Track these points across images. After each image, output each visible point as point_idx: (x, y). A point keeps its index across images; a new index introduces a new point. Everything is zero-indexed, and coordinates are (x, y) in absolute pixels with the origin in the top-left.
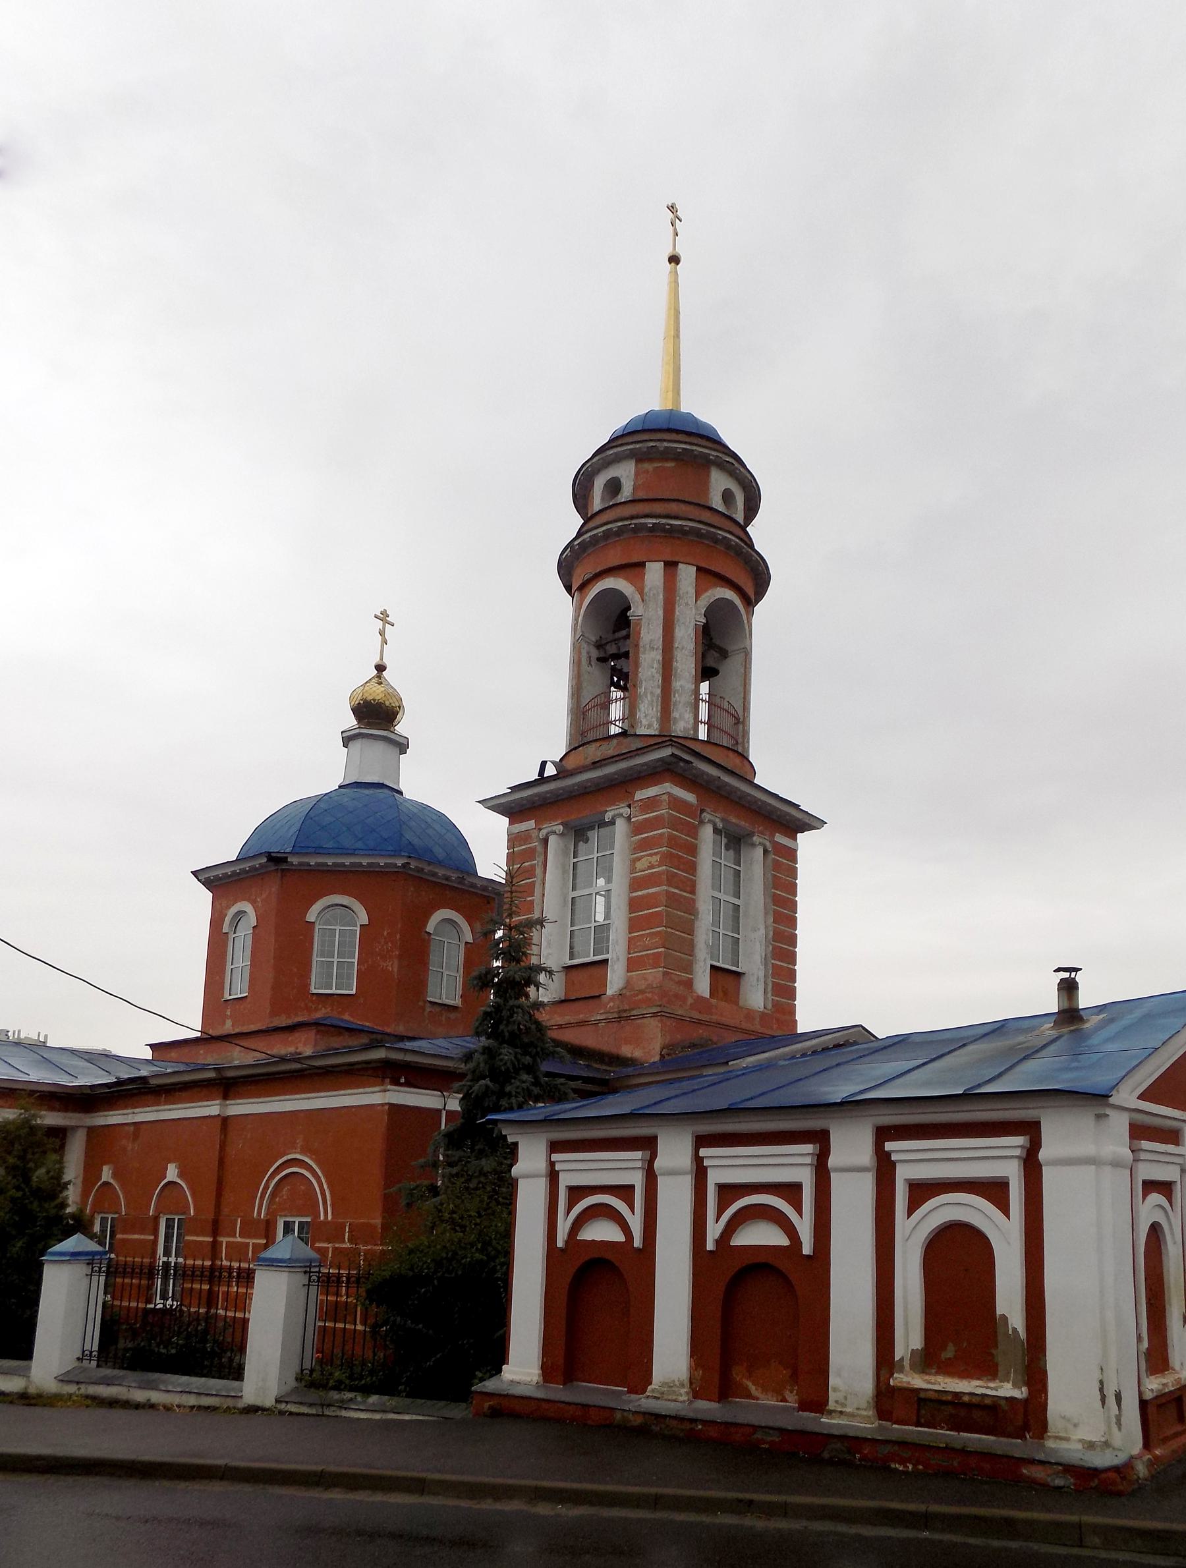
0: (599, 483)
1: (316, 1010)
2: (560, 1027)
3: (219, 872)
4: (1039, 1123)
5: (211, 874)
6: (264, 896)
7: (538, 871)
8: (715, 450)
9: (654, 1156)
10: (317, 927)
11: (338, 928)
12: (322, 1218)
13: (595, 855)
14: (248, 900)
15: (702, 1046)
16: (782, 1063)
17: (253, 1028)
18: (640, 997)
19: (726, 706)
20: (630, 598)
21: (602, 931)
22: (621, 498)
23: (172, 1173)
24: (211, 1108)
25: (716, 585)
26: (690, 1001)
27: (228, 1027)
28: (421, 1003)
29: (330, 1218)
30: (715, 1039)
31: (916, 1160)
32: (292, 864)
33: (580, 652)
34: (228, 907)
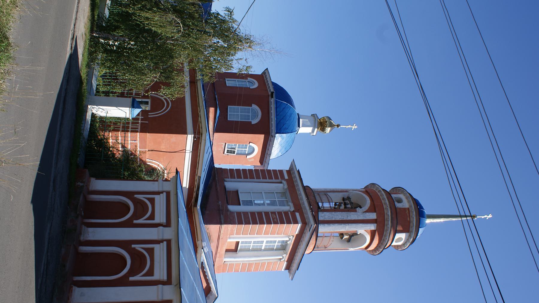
0: (401, 196)
3: (268, 77)
4: (170, 227)
5: (267, 74)
9: (164, 226)
10: (250, 108)
13: (277, 200)
19: (330, 242)
21: (249, 203)
22: (396, 203)
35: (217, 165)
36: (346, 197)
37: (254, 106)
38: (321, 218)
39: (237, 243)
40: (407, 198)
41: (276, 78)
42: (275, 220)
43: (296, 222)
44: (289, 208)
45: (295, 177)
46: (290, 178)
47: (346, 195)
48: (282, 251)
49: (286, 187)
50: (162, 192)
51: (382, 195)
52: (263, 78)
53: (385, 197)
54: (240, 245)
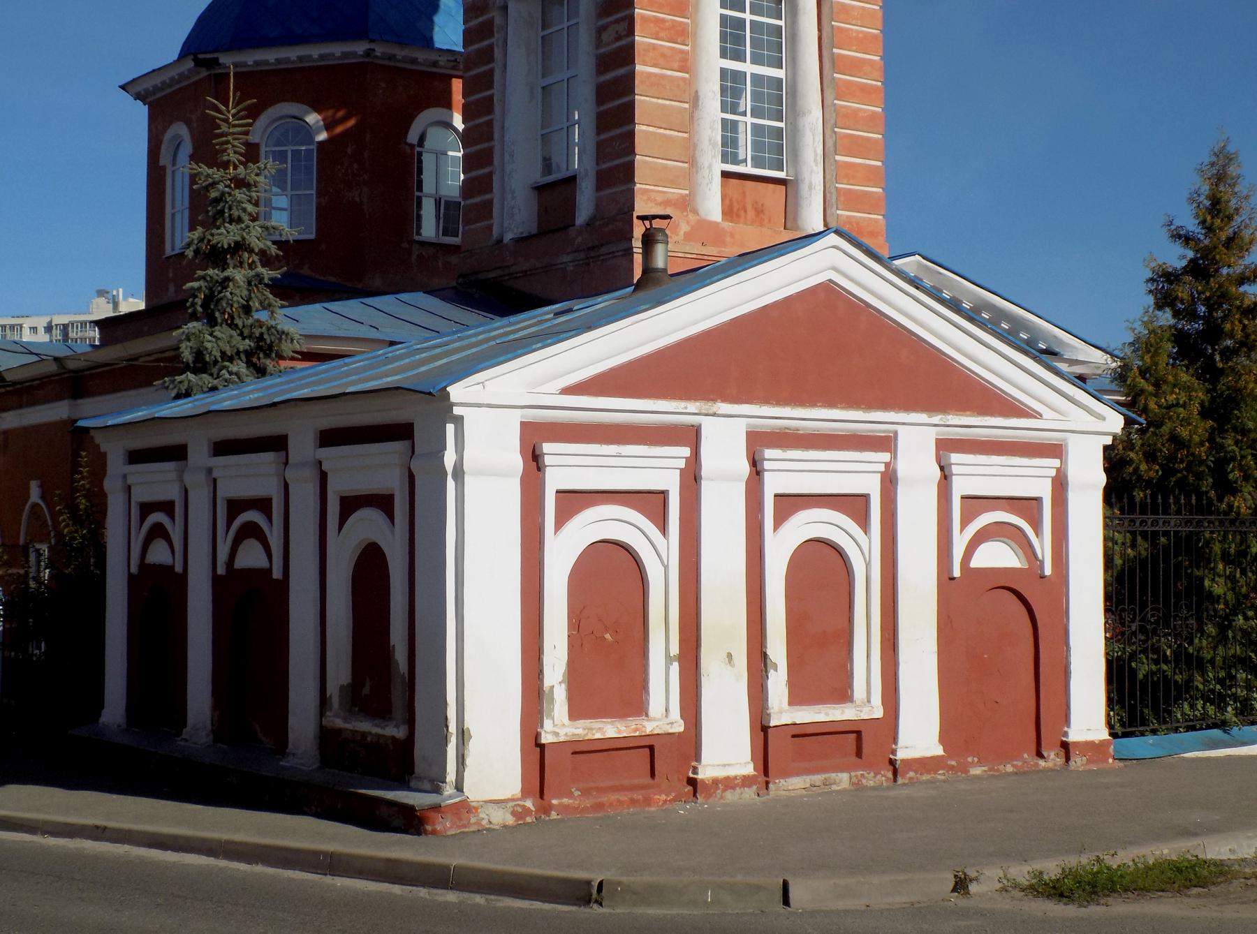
2: (525, 274)
5: (148, 84)
7: (497, 53)
11: (289, 148)
14: (178, 119)
18: (611, 227)
28: (405, 245)
31: (567, 467)
39: (726, 175)
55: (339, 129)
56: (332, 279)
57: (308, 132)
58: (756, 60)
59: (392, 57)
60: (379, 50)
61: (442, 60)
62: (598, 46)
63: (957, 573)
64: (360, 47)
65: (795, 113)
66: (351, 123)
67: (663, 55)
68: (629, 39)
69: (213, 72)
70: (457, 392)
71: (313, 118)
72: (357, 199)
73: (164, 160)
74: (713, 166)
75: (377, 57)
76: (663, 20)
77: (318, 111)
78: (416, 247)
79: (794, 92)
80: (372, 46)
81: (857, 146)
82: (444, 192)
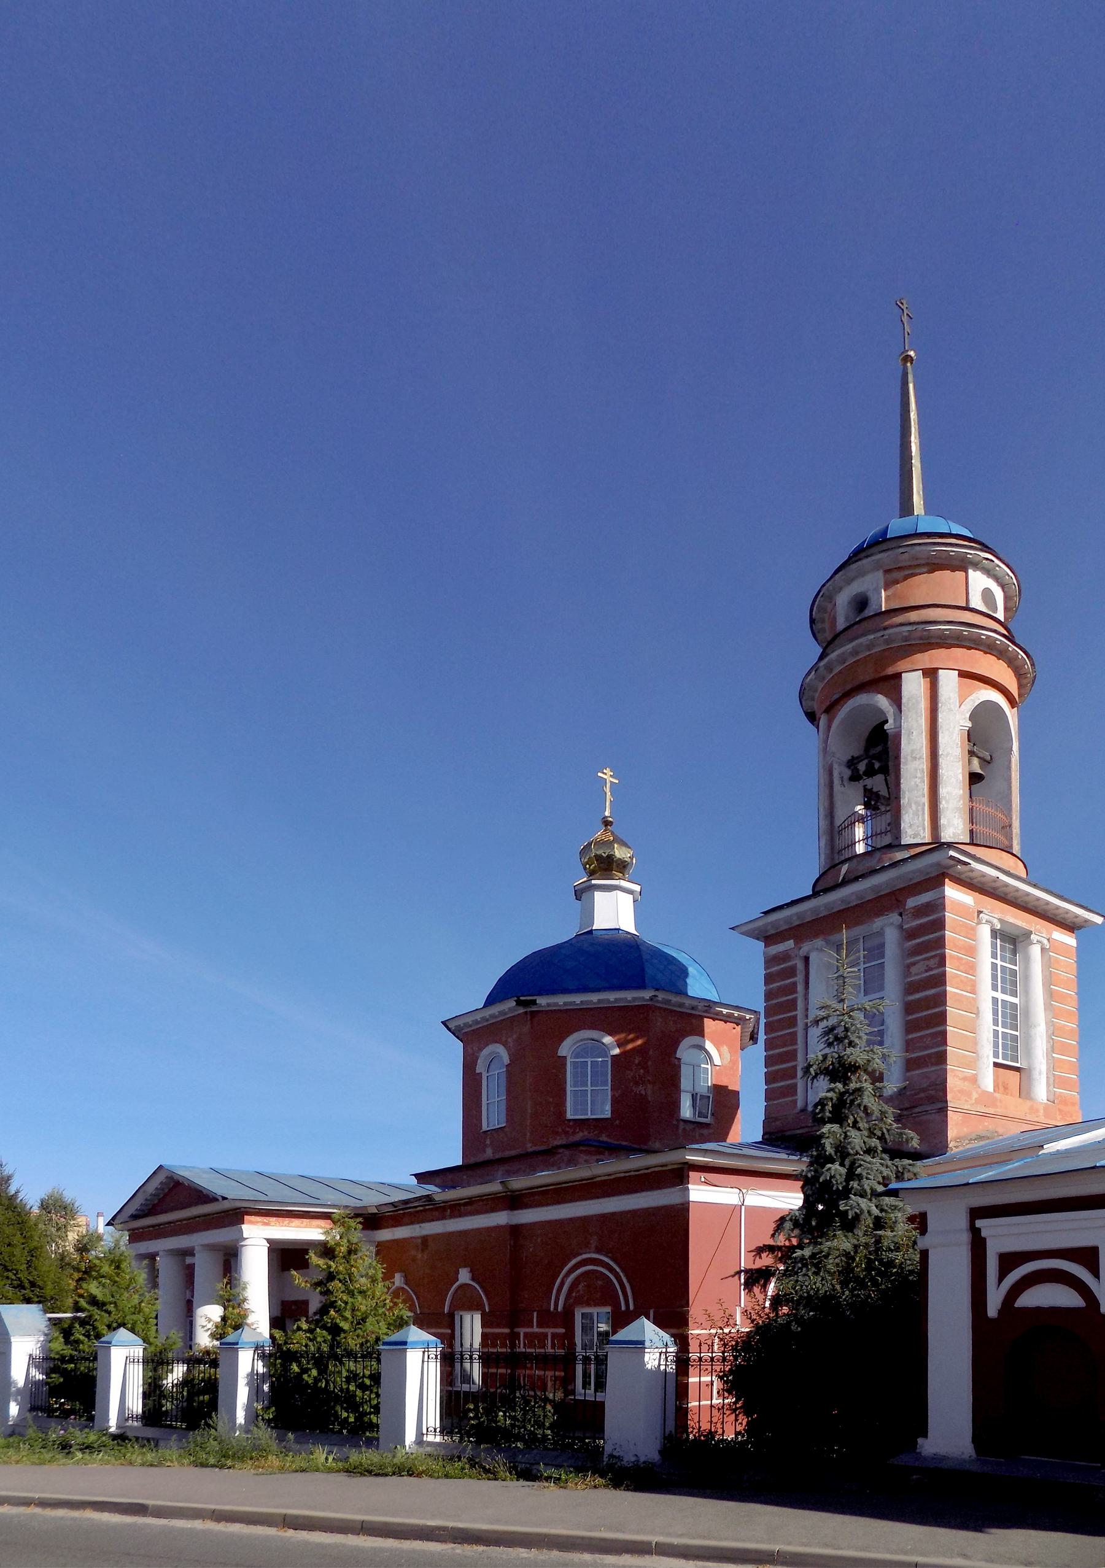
1: (574, 1133)
3: (469, 1020)
5: (460, 1022)
6: (515, 1036)
7: (800, 988)
8: (971, 548)
10: (569, 1061)
11: (589, 1060)
12: (623, 1308)
15: (988, 1138)
16: (210, 1314)
17: (513, 1153)
20: (885, 711)
23: (464, 1276)
24: (501, 1218)
25: (981, 689)
26: (975, 1095)
27: (489, 1154)
28: (675, 1122)
29: (632, 1307)
30: (1001, 1131)
32: (541, 1006)
33: (831, 774)
34: (481, 1050)
35: (760, 1139)
36: (848, 773)
37: (566, 1048)
38: (926, 836)
39: (996, 1065)
40: (849, 581)
41: (471, 996)
42: (932, 963)
43: (938, 906)
44: (889, 929)
45: (787, 920)
46: (787, 935)
47: (840, 771)
48: (1019, 946)
49: (819, 942)
50: (975, 1232)
51: (842, 659)
52: (471, 1034)
53: (849, 647)
54: (1000, 1061)
55: (630, 1046)
56: (624, 1143)
57: (604, 1049)
58: (1004, 992)
59: (668, 1002)
60: (661, 996)
61: (701, 1005)
62: (906, 977)
63: (992, 1311)
64: (647, 994)
65: (1028, 1025)
66: (639, 1042)
67: (962, 981)
68: (940, 970)
69: (529, 1010)
70: (246, 1217)
71: (608, 1040)
72: (643, 1092)
73: (480, 1068)
74: (987, 1058)
75: (658, 1001)
76: (961, 959)
77: (610, 1035)
78: (682, 1123)
79: (1027, 1013)
80: (656, 993)
81: (1064, 1049)
82: (697, 1090)
